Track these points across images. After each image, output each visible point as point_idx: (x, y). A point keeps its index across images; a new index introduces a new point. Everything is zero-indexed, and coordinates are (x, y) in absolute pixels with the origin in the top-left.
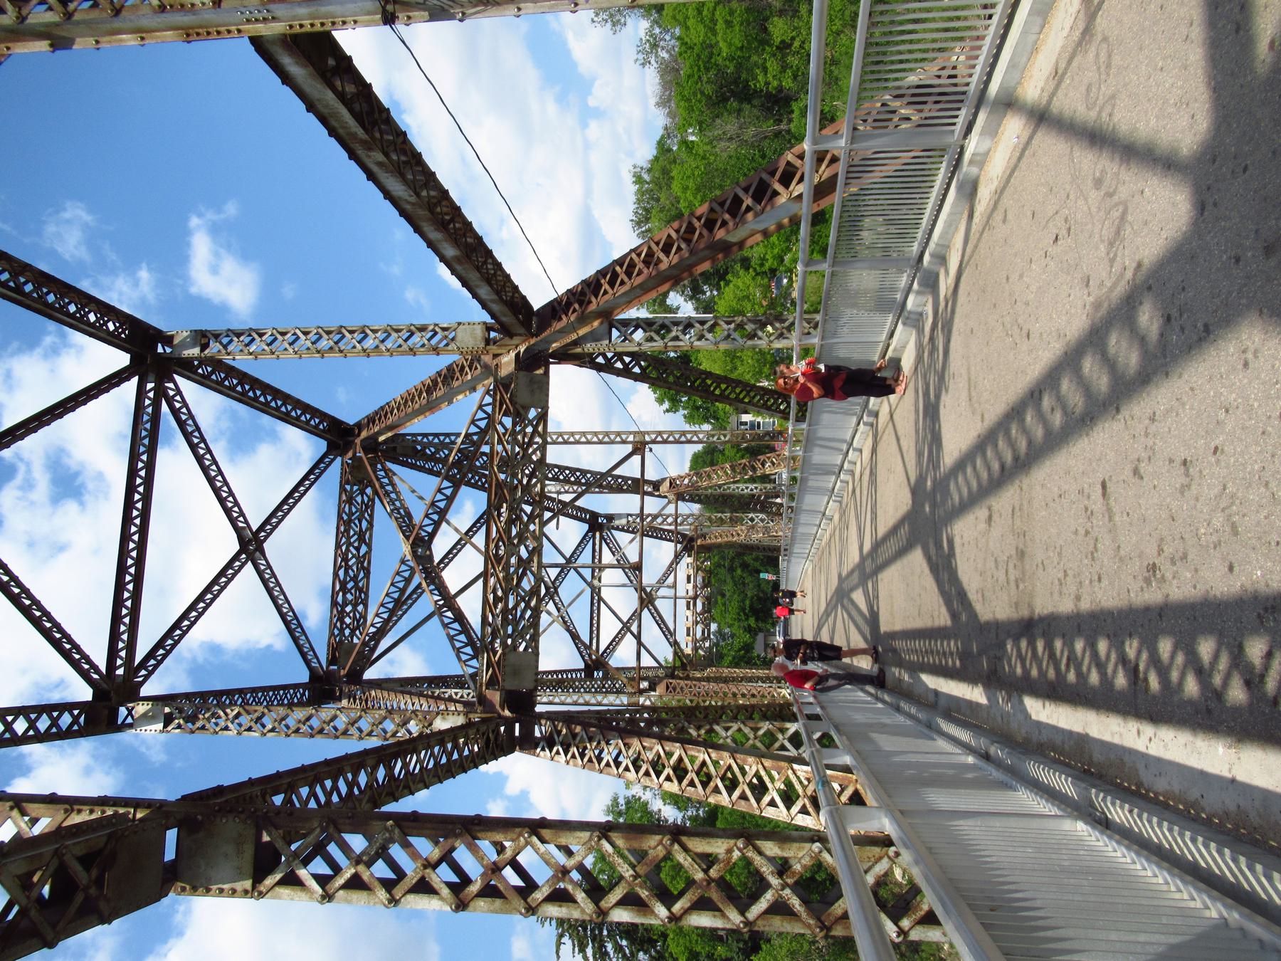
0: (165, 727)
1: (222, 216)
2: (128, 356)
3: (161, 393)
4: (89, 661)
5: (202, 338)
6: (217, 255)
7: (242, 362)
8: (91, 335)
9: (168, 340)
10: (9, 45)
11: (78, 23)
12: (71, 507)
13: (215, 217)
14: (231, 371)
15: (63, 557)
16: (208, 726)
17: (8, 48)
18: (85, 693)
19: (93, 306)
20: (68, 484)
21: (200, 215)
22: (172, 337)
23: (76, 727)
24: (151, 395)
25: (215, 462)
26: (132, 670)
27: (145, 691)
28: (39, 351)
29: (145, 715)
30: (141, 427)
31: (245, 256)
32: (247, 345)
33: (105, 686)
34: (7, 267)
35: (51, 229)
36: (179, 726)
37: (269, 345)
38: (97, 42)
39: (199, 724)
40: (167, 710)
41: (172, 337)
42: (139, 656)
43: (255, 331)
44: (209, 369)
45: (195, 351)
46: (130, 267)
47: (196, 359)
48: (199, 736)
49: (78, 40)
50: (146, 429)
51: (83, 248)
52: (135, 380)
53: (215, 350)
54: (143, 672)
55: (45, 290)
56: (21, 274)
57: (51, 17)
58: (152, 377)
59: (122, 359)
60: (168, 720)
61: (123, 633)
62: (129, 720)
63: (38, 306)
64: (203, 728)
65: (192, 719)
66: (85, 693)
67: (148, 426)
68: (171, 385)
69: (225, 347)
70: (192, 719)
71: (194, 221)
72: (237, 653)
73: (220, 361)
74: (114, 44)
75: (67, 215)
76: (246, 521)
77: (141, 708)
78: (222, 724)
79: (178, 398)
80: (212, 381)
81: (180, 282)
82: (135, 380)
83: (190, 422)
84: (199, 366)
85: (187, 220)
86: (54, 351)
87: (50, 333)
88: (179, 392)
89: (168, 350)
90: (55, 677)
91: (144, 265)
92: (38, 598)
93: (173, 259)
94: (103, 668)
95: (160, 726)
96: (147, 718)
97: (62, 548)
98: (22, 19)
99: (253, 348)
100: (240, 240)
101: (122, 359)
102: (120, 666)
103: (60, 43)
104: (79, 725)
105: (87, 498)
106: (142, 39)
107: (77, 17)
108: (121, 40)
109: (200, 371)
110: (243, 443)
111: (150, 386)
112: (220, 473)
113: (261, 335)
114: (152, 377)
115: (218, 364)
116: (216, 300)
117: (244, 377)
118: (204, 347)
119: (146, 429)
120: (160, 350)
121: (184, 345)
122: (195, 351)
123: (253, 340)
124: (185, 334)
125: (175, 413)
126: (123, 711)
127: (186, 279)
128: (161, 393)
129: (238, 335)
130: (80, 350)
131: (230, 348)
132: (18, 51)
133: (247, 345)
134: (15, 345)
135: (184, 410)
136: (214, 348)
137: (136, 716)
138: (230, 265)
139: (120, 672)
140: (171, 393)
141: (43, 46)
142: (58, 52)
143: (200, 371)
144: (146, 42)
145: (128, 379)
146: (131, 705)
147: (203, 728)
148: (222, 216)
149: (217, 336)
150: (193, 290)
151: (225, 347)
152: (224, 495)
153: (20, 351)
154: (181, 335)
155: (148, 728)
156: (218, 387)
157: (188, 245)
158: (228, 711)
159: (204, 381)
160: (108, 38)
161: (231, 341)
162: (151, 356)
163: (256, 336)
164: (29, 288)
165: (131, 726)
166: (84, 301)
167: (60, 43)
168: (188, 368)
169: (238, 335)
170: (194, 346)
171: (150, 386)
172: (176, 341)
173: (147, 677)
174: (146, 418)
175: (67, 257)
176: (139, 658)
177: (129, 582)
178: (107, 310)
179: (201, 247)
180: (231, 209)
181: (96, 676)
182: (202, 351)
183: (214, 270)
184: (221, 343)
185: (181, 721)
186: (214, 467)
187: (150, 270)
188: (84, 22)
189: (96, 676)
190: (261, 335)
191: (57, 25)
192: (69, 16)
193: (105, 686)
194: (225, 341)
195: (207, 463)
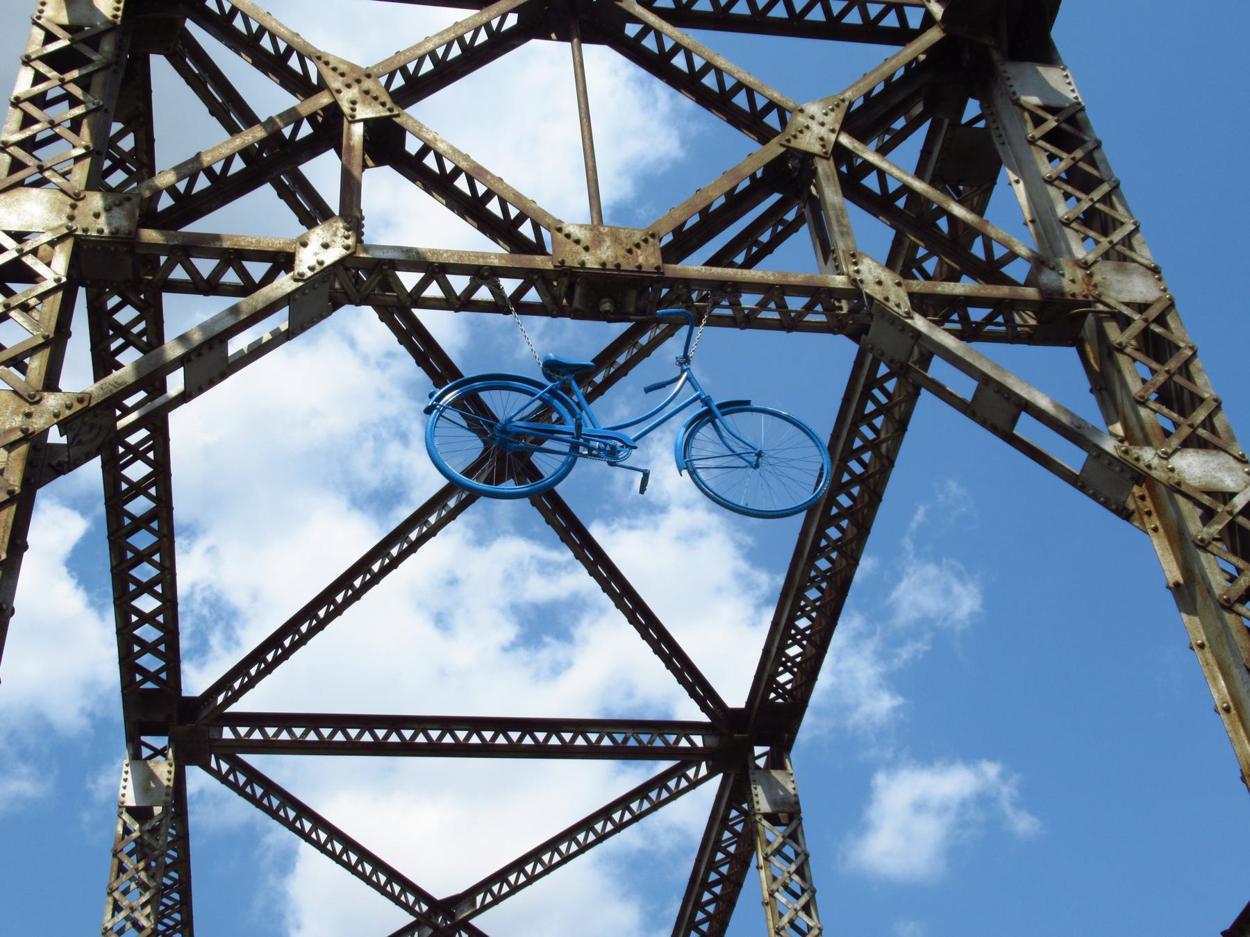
0: (130, 810)
1: (1009, 810)
2: (742, 705)
3: (689, 757)
4: (244, 689)
5: (788, 813)
6: (942, 810)
7: (757, 881)
8: (766, 651)
9: (777, 761)
10: (1161, 530)
11: (1222, 619)
12: (509, 631)
13: (1006, 805)
14: (741, 863)
15: (429, 631)
16: (124, 877)
17: (1155, 530)
18: (196, 681)
19: (812, 651)
20: (543, 626)
21: (1003, 776)
22: (782, 767)
23: (138, 678)
24: (684, 743)
25: (601, 838)
26: (229, 752)
27: (196, 778)
28: (744, 566)
29: (152, 776)
30: (630, 732)
31: (953, 852)
32: (786, 887)
33: (205, 712)
34: (849, 536)
35: (931, 570)
36: (127, 831)
37: (792, 923)
38: (1202, 646)
39: (129, 863)
40: (158, 810)
41: (782, 767)
42: (253, 760)
43: (812, 898)
44: (739, 828)
45: (763, 805)
46: (894, 681)
47: (752, 807)
48: (110, 864)
49: (1197, 619)
50: (626, 740)
51: (915, 615)
52: (704, 718)
53: (770, 836)
54: (225, 767)
55: (824, 585)
56: (842, 554)
57: (1218, 582)
58: (713, 741)
59: (735, 695)
60: (140, 813)
61: (291, 733)
62: (146, 752)
63: (797, 578)
64: (121, 869)
65: (142, 850)
66: (196, 681)
67: (632, 742)
68: (703, 771)
69: (778, 851)
70: (142, 850)
71: (991, 770)
72: (283, 896)
73: (753, 847)
74: (1205, 670)
75: (957, 588)
76: (485, 907)
77: (163, 770)
78: (125, 902)
79: (684, 783)
80: (720, 834)
81: (889, 755)
82: (704, 718)
83: (646, 805)
84: (742, 812)
85: (992, 758)
86: (748, 586)
87: (773, 579)
88: (694, 784)
89: (761, 762)
90: (240, 633)
91: (899, 700)
92: (346, 613)
93: (922, 742)
94: (234, 708)
95: (131, 801)
96: (146, 781)
97: (442, 621)
98: (1203, 546)
99: (782, 898)
100: (975, 838)
101: (735, 695)
102: (236, 733)
103: (1187, 592)
104: (143, 682)
105: (522, 653)
106: (1227, 710)
107: (1229, 618)
108: (1215, 679)
109: (734, 813)
110: (636, 875)
111: (698, 740)
112: (583, 849)
113: (806, 909)
114: (713, 741)
115: (748, 841)
116: (872, 813)
117: (734, 883)
118: (773, 819)
119: (626, 740)
120: (758, 750)
121: (771, 787)
122: (763, 805)
123: (797, 897)
124: (790, 787)
125: (659, 782)
126: (160, 742)
127: (892, 766)
128: (689, 757)
129: (800, 872)
130: (754, 624)
131: (777, 861)
132: (1155, 542)
133: (786, 887)
134: (749, 540)
135: (665, 795)
136: (773, 834)
137: (151, 764)
138: (930, 831)
139: (227, 733)
140: (691, 773)
141: (1173, 573)
142: (1169, 594)
143: (734, 813)
144: (1223, 716)
145: (704, 708)
146: (170, 753)
147: (121, 869)
148: (1009, 810)
149: (793, 837)
150: (880, 779)
151: (778, 851)
152: (529, 868)
153: (740, 546)
154: (787, 781)
155: (130, 784)
156: (711, 841)
157: (952, 762)
158: (148, 909)
159: (718, 820)
160: (1212, 660)
161: (789, 861)
162: (747, 739)
163: (803, 900)
164: (823, 564)
165: (136, 756)
166: (817, 639)
167: (1187, 592)
168: (734, 795)
169: (800, 872)
170: (772, 802)
171: (698, 740)
172: (776, 774)
173: (217, 774)
174: (645, 738)
175: (895, 594)
176: (251, 759)
177: (374, 735)
178: (809, 671)
179: (953, 783)
180: (1024, 824)
181: (220, 699)
182: (767, 816)
183: (920, 807)
184: (783, 844)
185: (136, 835)
186: (574, 848)
187: (896, 710)
188: (1225, 625)
189: (220, 699)
190: (806, 909)
191: (1209, 590)
192: (1228, 606)
193: (205, 712)
194: (788, 851)
195: (581, 837)
